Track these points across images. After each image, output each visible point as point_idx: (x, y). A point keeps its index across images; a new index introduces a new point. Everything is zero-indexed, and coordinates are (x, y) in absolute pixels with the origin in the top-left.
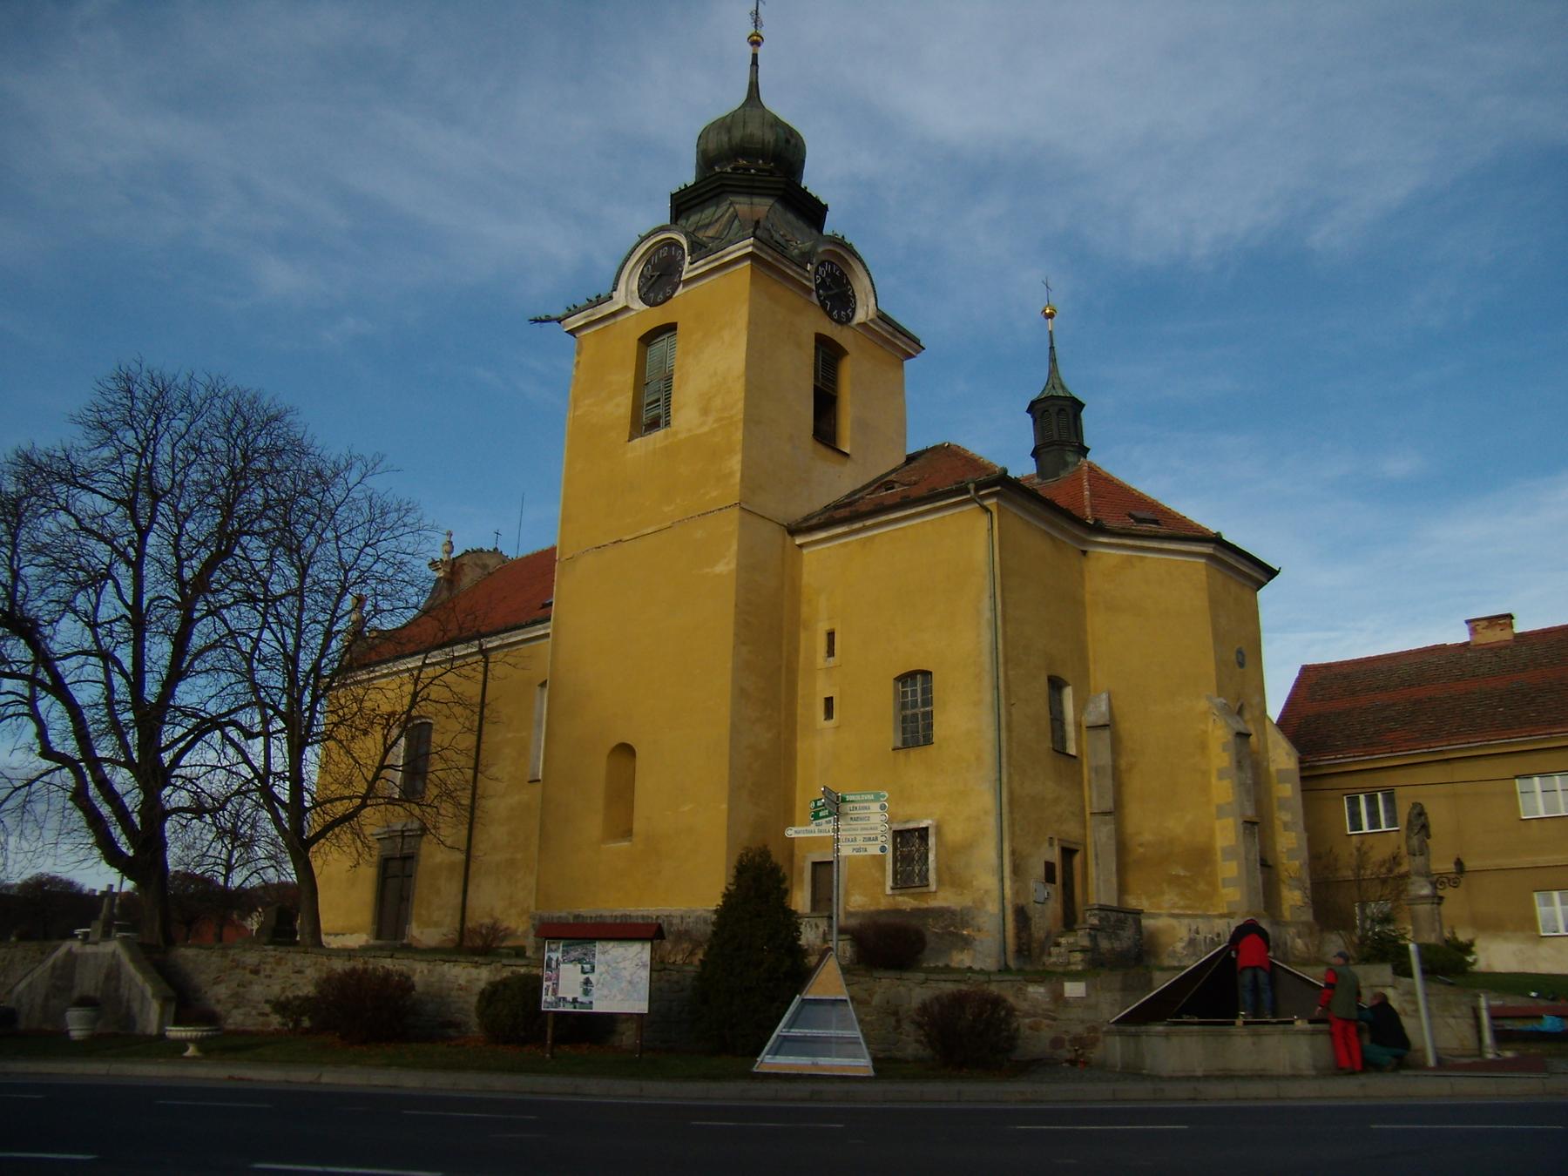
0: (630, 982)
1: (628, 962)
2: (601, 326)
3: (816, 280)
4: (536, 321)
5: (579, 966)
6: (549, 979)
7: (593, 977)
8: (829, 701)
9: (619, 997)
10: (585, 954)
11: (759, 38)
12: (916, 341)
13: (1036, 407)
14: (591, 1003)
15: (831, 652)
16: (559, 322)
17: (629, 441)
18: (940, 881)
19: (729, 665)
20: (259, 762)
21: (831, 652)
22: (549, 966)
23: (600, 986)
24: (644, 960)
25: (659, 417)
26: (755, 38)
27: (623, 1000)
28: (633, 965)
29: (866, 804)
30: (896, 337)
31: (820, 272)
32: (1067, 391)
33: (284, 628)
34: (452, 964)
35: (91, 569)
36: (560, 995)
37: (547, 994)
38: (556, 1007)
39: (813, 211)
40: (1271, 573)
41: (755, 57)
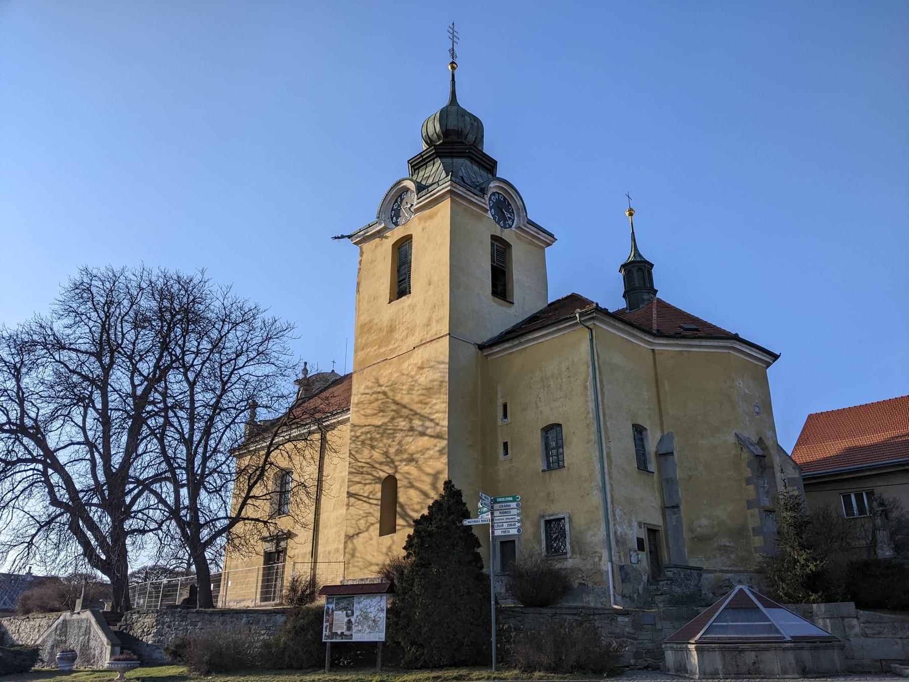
0: (374, 621)
1: (372, 609)
2: (550, 337)
3: (490, 204)
4: (336, 238)
5: (345, 612)
6: (327, 621)
7: (353, 620)
8: (505, 444)
9: (368, 631)
10: (348, 604)
12: (552, 236)
14: (352, 635)
15: (505, 416)
16: (349, 238)
17: (389, 303)
18: (573, 552)
20: (171, 500)
21: (505, 416)
22: (327, 613)
23: (356, 624)
24: (382, 606)
25: (406, 289)
27: (370, 632)
28: (376, 610)
29: (509, 504)
30: (539, 234)
31: (492, 199)
32: (643, 258)
34: (281, 615)
35: (257, 439)
36: (334, 631)
37: (326, 631)
38: (331, 639)
39: (489, 165)
40: (775, 357)
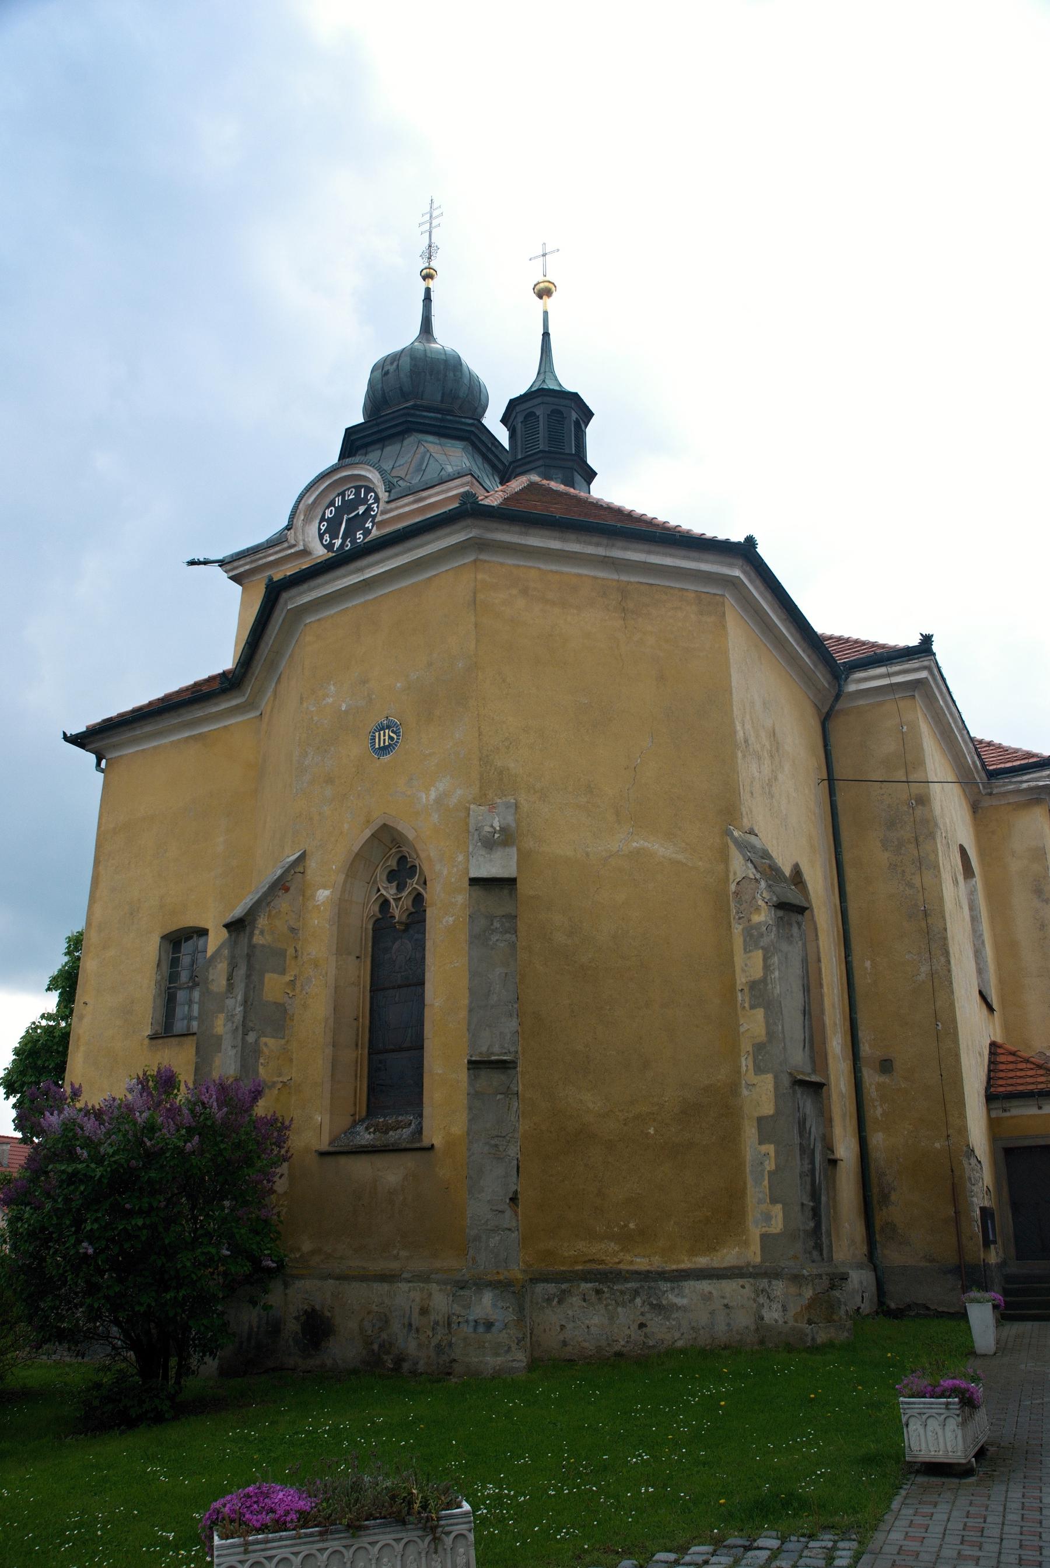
11: (432, 271)
13: (518, 409)
19: (839, 808)
26: (428, 270)
33: (755, 1544)
41: (428, 291)
